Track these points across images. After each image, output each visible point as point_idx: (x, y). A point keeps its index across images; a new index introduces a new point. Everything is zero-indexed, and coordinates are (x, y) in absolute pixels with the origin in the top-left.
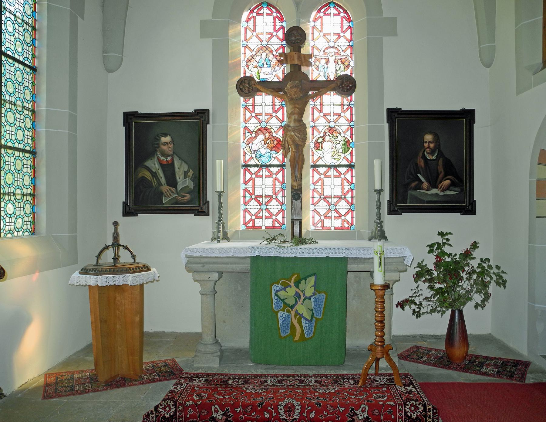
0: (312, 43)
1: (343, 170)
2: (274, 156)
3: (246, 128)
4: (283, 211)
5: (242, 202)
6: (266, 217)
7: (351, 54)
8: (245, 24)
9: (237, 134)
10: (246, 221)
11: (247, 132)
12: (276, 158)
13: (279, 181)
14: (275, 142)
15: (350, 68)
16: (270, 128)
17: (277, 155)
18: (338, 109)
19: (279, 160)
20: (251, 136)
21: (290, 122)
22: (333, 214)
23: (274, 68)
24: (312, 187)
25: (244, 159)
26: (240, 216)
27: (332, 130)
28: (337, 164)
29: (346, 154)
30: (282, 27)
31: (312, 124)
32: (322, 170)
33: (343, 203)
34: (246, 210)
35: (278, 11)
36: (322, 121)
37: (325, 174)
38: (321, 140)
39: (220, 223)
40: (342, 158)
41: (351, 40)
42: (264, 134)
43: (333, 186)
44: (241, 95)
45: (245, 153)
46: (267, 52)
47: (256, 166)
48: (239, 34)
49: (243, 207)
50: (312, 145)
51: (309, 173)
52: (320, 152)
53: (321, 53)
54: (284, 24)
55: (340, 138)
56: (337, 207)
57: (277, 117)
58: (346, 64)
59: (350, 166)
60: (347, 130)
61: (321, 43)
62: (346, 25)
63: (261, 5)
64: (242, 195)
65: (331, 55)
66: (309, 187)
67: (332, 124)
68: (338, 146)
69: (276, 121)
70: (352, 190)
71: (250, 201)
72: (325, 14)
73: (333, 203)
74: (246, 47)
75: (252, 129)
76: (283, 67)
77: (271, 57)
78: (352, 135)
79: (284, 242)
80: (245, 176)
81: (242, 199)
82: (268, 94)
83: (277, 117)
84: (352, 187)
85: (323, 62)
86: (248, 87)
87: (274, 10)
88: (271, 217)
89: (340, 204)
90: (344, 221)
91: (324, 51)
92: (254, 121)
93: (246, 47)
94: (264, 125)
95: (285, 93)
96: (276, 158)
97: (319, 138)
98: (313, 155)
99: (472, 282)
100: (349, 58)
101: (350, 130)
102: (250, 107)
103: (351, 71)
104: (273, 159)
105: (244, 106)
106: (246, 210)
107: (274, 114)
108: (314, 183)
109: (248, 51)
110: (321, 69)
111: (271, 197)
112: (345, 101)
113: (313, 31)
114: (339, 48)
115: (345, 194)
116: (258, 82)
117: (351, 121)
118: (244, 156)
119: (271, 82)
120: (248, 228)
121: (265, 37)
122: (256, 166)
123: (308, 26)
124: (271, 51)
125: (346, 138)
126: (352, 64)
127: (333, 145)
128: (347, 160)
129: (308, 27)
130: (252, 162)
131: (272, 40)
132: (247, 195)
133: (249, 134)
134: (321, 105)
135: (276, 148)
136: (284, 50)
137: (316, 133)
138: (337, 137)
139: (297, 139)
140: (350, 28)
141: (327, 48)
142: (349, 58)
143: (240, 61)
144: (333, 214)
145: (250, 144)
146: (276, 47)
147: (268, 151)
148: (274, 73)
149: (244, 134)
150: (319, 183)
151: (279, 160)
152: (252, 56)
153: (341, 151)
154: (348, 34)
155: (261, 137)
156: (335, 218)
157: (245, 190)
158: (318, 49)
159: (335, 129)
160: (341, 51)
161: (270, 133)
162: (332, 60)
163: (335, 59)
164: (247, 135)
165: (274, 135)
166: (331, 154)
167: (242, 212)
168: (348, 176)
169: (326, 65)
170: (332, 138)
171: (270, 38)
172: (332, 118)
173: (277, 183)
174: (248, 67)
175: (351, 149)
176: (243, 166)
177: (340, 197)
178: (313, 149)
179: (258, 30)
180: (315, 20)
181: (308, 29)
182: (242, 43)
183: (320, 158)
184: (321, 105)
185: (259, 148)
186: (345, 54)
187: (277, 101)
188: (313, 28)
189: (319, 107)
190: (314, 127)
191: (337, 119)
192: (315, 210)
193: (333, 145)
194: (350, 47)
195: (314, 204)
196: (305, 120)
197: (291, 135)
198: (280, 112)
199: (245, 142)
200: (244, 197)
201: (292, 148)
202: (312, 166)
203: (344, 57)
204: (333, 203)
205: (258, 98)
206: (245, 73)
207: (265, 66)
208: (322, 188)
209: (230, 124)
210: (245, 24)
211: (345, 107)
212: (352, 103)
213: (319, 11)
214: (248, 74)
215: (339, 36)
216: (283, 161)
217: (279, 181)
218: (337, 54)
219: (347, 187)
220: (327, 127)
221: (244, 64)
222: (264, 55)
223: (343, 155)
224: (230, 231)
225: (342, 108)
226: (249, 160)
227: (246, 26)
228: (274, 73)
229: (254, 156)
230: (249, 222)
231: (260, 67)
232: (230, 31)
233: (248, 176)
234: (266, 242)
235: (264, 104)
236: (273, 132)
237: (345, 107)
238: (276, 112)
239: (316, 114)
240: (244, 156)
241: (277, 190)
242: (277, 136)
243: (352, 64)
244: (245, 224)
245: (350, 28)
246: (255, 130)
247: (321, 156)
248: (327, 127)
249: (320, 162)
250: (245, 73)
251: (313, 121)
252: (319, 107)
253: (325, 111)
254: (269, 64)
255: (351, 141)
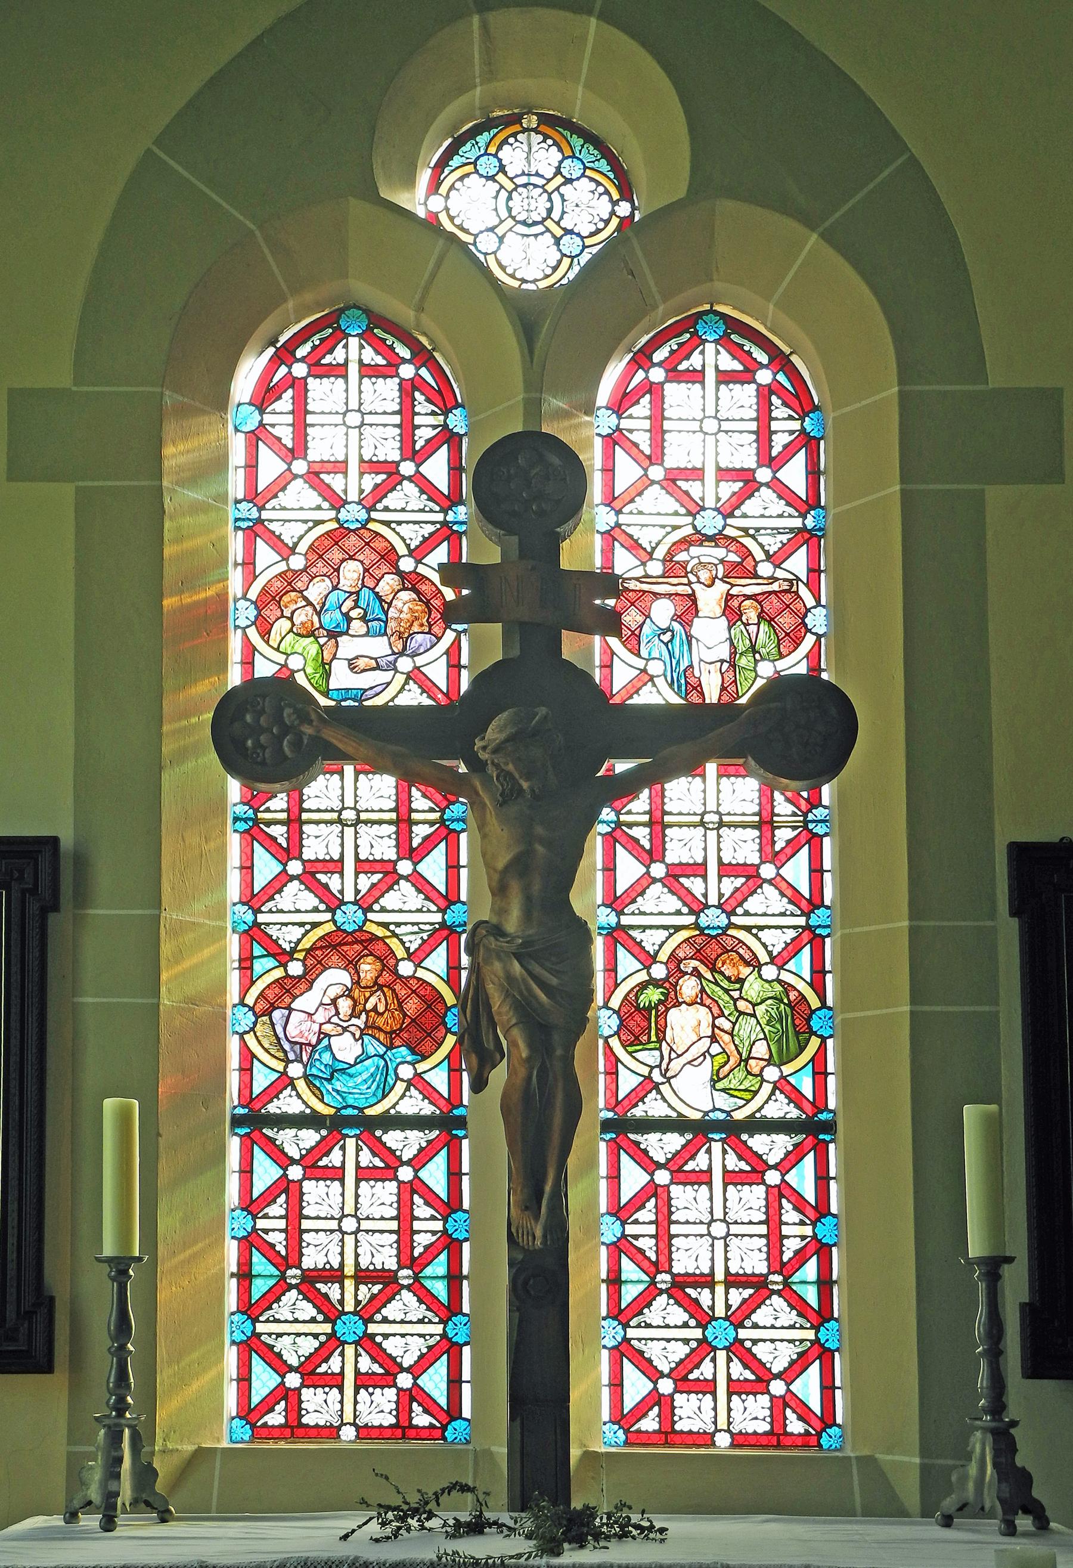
0: (604, 518)
1: (772, 1147)
2: (406, 1072)
3: (254, 933)
4: (450, 1348)
5: (231, 1301)
6: (363, 1381)
7: (814, 571)
8: (251, 419)
9: (206, 961)
10: (255, 1400)
11: (258, 950)
12: (418, 1082)
13: (430, 1197)
14: (412, 1006)
15: (809, 641)
16: (380, 932)
17: (421, 1067)
18: (743, 847)
19: (429, 1092)
20: (279, 973)
21: (501, 911)
22: (719, 1368)
23: (404, 637)
24: (610, 1230)
25: (247, 1084)
26: (220, 1375)
27: (711, 950)
28: (739, 1115)
29: (787, 1069)
30: (447, 437)
31: (606, 917)
32: (663, 1145)
33: (775, 1312)
34: (252, 1346)
35: (422, 356)
36: (659, 902)
37: (676, 1165)
38: (653, 995)
39: (123, 1413)
40: (767, 1088)
41: (812, 503)
42: (352, 965)
43: (719, 1227)
44: (231, 766)
45: (248, 1058)
46: (369, 556)
47: (310, 1120)
48: (219, 463)
49: (236, 1327)
50: (608, 1023)
51: (594, 1163)
52: (650, 1057)
53: (655, 568)
54: (457, 421)
55: (753, 988)
56: (743, 1334)
57: (420, 883)
58: (786, 621)
59: (812, 1129)
60: (793, 949)
61: (654, 518)
62: (785, 427)
63: (330, 328)
64: (232, 1264)
65: (704, 576)
66: (593, 1229)
67: (713, 918)
68: (747, 1028)
69: (416, 900)
70: (822, 1250)
71: (273, 1296)
72: (674, 375)
73: (349, 896)
74: (255, 530)
75: (287, 937)
76: (449, 636)
77: (388, 583)
78: (818, 972)
79: (477, 1527)
80: (247, 1171)
81: (232, 1286)
82: (376, 768)
83: (420, 883)
84: (826, 1231)
85: (663, 612)
86: (275, 735)
87: (404, 352)
88: (387, 1380)
89: (762, 1316)
90: (780, 1405)
91: (669, 558)
92: (296, 897)
93: (255, 530)
94: (349, 918)
95: (476, 765)
96: (418, 1082)
97: (643, 986)
98: (613, 1073)
99: (74, 389)
100: (804, 592)
101: (806, 951)
102: (278, 832)
103: (813, 656)
104: (400, 1087)
105: (242, 826)
106: (252, 1346)
107: (405, 867)
108: (621, 1212)
109: (265, 554)
110: (653, 647)
111: (387, 1279)
112: (783, 807)
113: (609, 457)
114: (748, 542)
115: (787, 1269)
116: (327, 709)
117: (815, 902)
118: (246, 1070)
119: (388, 711)
120: (261, 1433)
121: (353, 484)
122: (310, 1120)
123: (585, 432)
124: (390, 556)
125: (787, 987)
126: (817, 620)
127: (722, 1022)
128: (795, 1096)
129: (589, 435)
130: (288, 1104)
131: (393, 500)
132: (260, 1264)
133: (271, 962)
134: (650, 824)
135: (417, 1032)
136: (455, 551)
137: (627, 963)
138: (741, 981)
139: (542, 997)
140: (807, 442)
141: (685, 543)
142: (804, 592)
143: (222, 598)
144: (719, 1368)
145: (277, 1015)
146: (414, 535)
147: (373, 1047)
148: (405, 664)
149: (246, 963)
150: (647, 1214)
151: (429, 1092)
152: (289, 578)
153: (761, 1050)
154: (795, 474)
155: (334, 979)
156: (736, 1388)
157: (251, 1242)
158: (634, 546)
159: (729, 942)
160: (759, 555)
161: (386, 961)
162: (710, 600)
163: (729, 597)
164: (259, 966)
165: (406, 968)
166: (706, 1069)
167: (231, 1356)
168: (803, 1178)
169: (676, 626)
170: (710, 988)
171: (380, 492)
172: (714, 888)
173: (422, 1210)
174: (265, 634)
175: (815, 1042)
176: (237, 1121)
177: (758, 1284)
178: (615, 1043)
179: (319, 448)
180: (621, 403)
181: (589, 445)
182: (232, 513)
183: (648, 1086)
184: (650, 824)
185: (322, 1035)
186: (780, 574)
187: (419, 802)
188: (614, 440)
189: (641, 834)
190: (617, 935)
191: (741, 897)
192: (624, 1351)
193: (722, 1022)
194: (805, 537)
195: (620, 1315)
196: (578, 904)
197: (510, 978)
198: (439, 854)
199: (250, 1000)
200: (245, 1276)
201: (512, 1044)
202: (607, 1126)
203: (775, 587)
204: (349, 896)
205: (322, 791)
206: (248, 662)
207: (357, 627)
208: (664, 1238)
209: (170, 915)
210: (251, 419)
211: (783, 836)
212: (819, 813)
213: (642, 359)
214: (264, 669)
215: (749, 485)
216: (454, 1099)
217: (430, 1197)
218: (742, 568)
219: (795, 1232)
220: (684, 934)
221: (245, 613)
222: (351, 572)
223: (772, 1074)
224: (170, 1447)
225: (766, 842)
226: (272, 1092)
227: (252, 425)
228: (405, 664)
229: (295, 1070)
230: (268, 1405)
231: (333, 635)
232: (168, 451)
233: (266, 1172)
234: (374, 1528)
235: (349, 815)
236: (400, 953)
237: (783, 836)
238: (416, 855)
239: (629, 871)
240: (246, 1070)
241: (422, 1240)
242: (421, 973)
243: (817, 620)
244: (248, 1413)
245: (807, 442)
246: (306, 944)
247: (656, 1076)
248: (684, 934)
249: (653, 1108)
250: (248, 662)
251: (615, 902)
252: (641, 834)
253: (674, 855)
254: (377, 623)
255: (814, 1002)
